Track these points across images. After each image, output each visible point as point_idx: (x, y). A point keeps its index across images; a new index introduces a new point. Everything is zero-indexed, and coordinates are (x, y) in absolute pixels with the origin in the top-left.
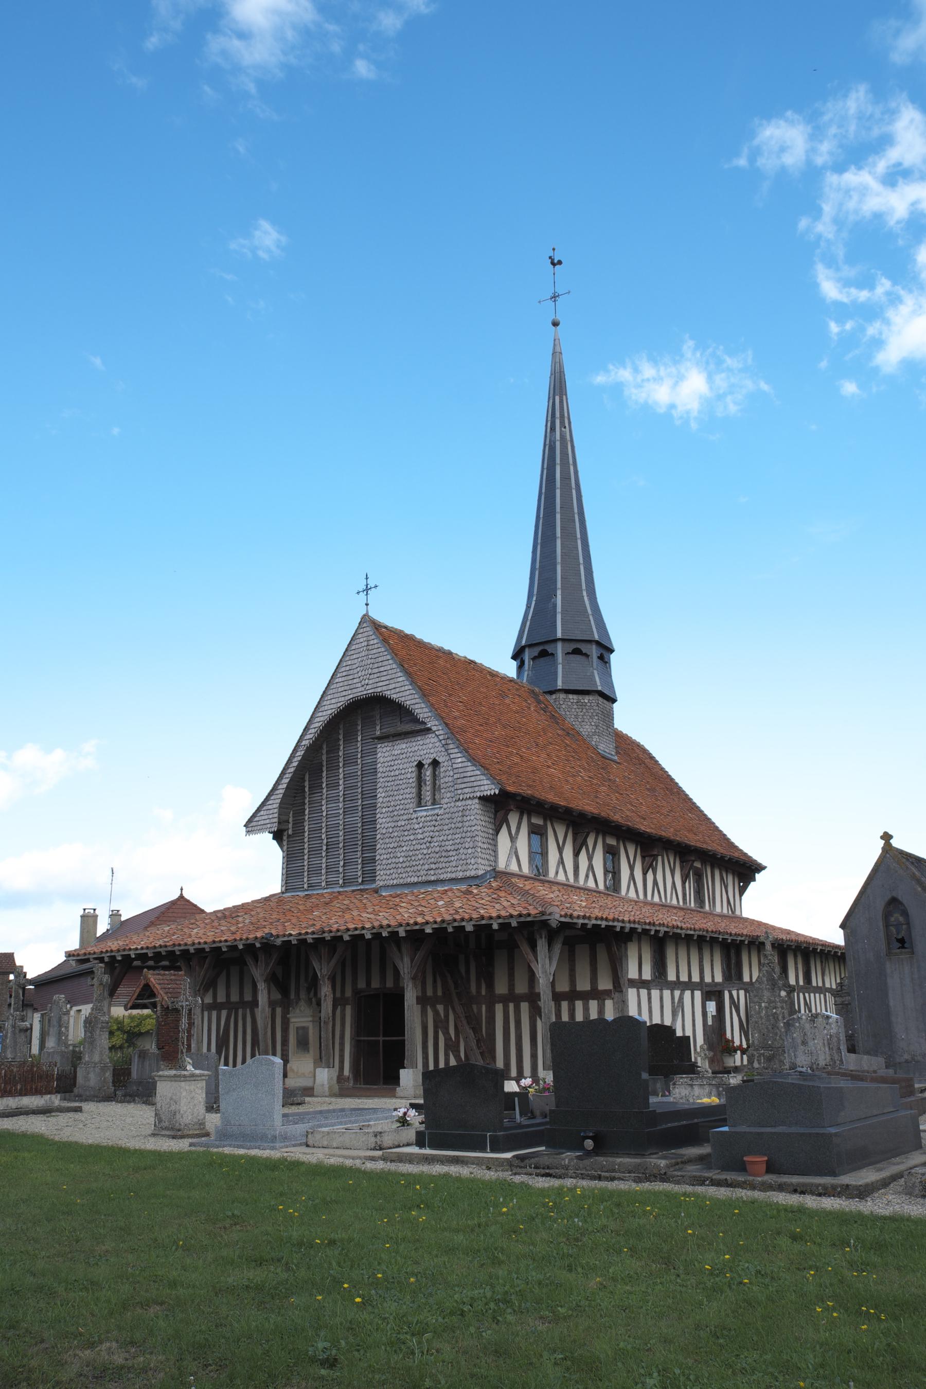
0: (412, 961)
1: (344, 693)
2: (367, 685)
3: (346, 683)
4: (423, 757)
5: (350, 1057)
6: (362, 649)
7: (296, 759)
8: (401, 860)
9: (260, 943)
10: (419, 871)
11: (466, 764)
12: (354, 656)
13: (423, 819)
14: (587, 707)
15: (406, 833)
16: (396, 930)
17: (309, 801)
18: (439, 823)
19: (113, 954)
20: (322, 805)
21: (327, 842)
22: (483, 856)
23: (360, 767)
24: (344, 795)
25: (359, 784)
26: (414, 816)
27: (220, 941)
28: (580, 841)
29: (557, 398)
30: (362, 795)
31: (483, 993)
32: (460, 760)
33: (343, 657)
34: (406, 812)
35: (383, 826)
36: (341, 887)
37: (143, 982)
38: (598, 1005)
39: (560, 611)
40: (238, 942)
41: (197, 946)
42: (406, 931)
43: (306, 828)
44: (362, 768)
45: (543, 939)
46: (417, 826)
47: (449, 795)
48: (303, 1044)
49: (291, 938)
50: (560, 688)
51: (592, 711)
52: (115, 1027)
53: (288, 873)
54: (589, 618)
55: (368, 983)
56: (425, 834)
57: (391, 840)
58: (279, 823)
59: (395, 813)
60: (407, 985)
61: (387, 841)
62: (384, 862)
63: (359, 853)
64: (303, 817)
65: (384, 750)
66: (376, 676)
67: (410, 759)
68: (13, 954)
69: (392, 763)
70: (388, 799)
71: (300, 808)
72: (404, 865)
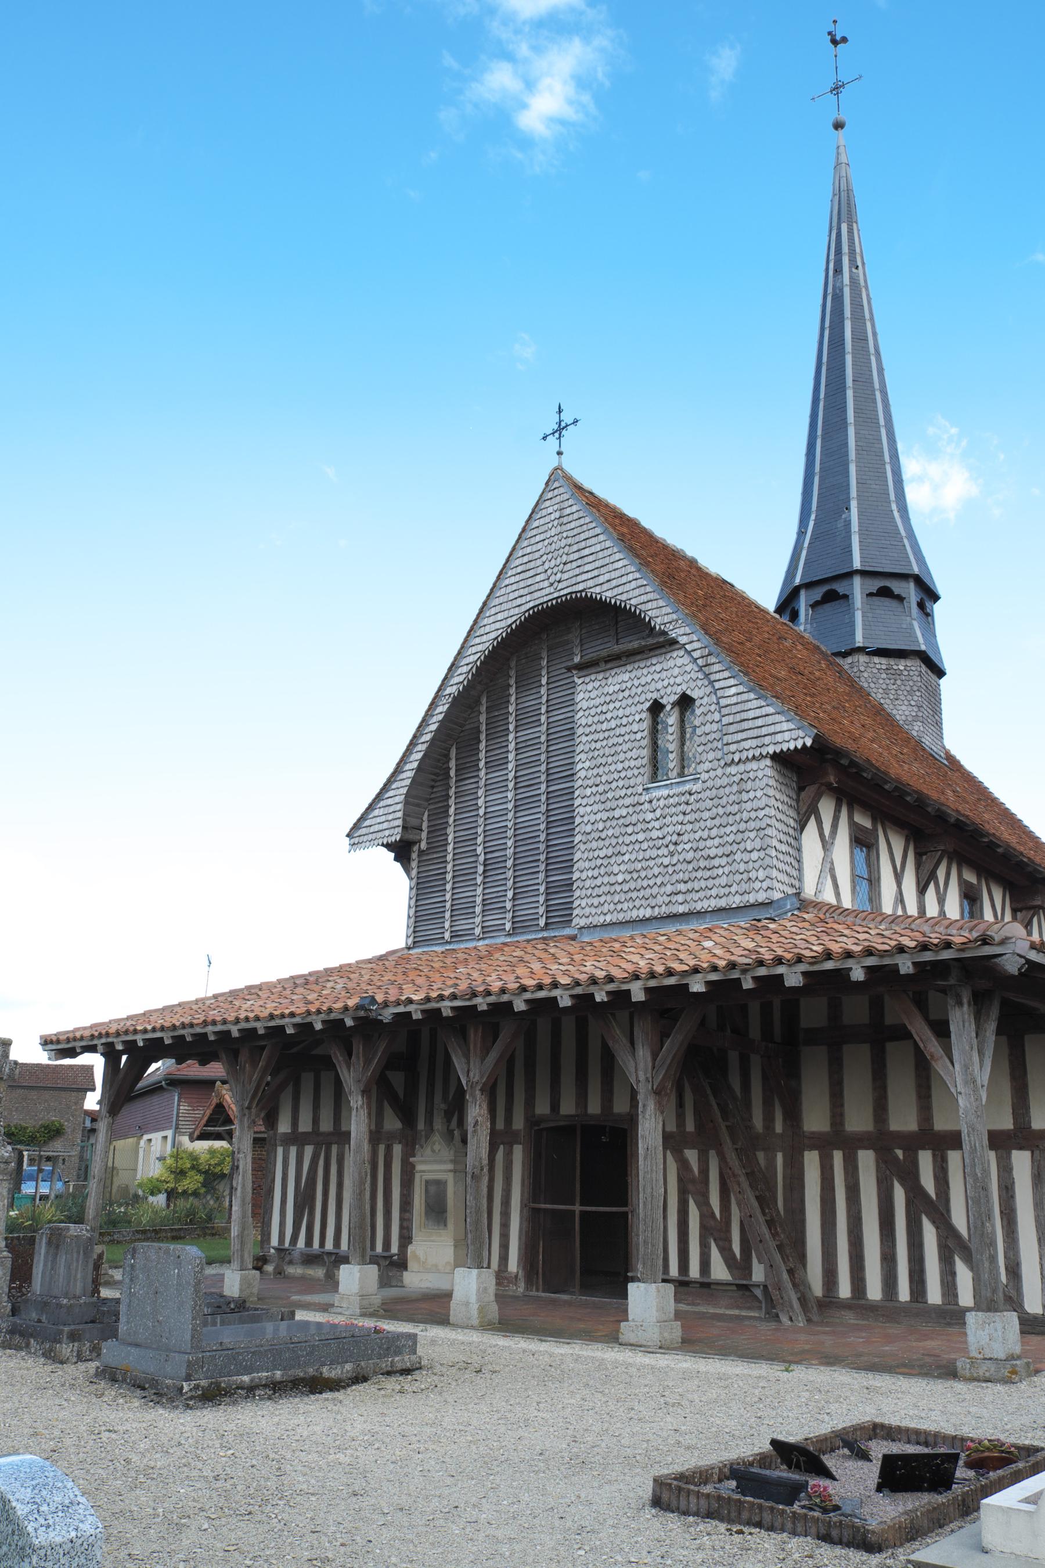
0: (655, 1056)
1: (519, 601)
2: (559, 582)
3: (522, 584)
4: (662, 692)
5: (520, 1238)
6: (550, 525)
7: (434, 719)
8: (620, 878)
9: (354, 1019)
10: (655, 897)
11: (745, 697)
12: (538, 539)
13: (662, 802)
14: (904, 678)
15: (630, 830)
16: (625, 987)
17: (456, 793)
18: (694, 807)
19: (110, 1040)
20: (478, 798)
21: (485, 860)
22: (781, 866)
23: (544, 728)
24: (516, 778)
25: (543, 757)
26: (646, 797)
27: (283, 1016)
28: (928, 867)
29: (844, 227)
30: (548, 775)
31: (779, 1128)
32: (733, 690)
33: (517, 541)
34: (629, 792)
35: (586, 819)
36: (509, 935)
37: (215, 1101)
38: (1033, 1162)
39: (857, 530)
40: (314, 1017)
41: (243, 1025)
42: (648, 990)
43: (450, 838)
44: (548, 729)
45: (965, 1007)
46: (650, 816)
47: (711, 756)
48: (437, 1211)
49: (411, 1008)
50: (861, 645)
51: (911, 683)
52: (189, 1166)
53: (419, 914)
54: (902, 541)
55: (555, 1107)
56: (666, 830)
57: (601, 843)
58: (405, 828)
59: (610, 795)
60: (644, 1106)
61: (594, 845)
62: (588, 883)
63: (542, 876)
64: (445, 821)
65: (590, 687)
66: (575, 564)
67: (637, 699)
68: (93, 1066)
69: (604, 708)
70: (595, 771)
71: (440, 805)
72: (626, 887)
